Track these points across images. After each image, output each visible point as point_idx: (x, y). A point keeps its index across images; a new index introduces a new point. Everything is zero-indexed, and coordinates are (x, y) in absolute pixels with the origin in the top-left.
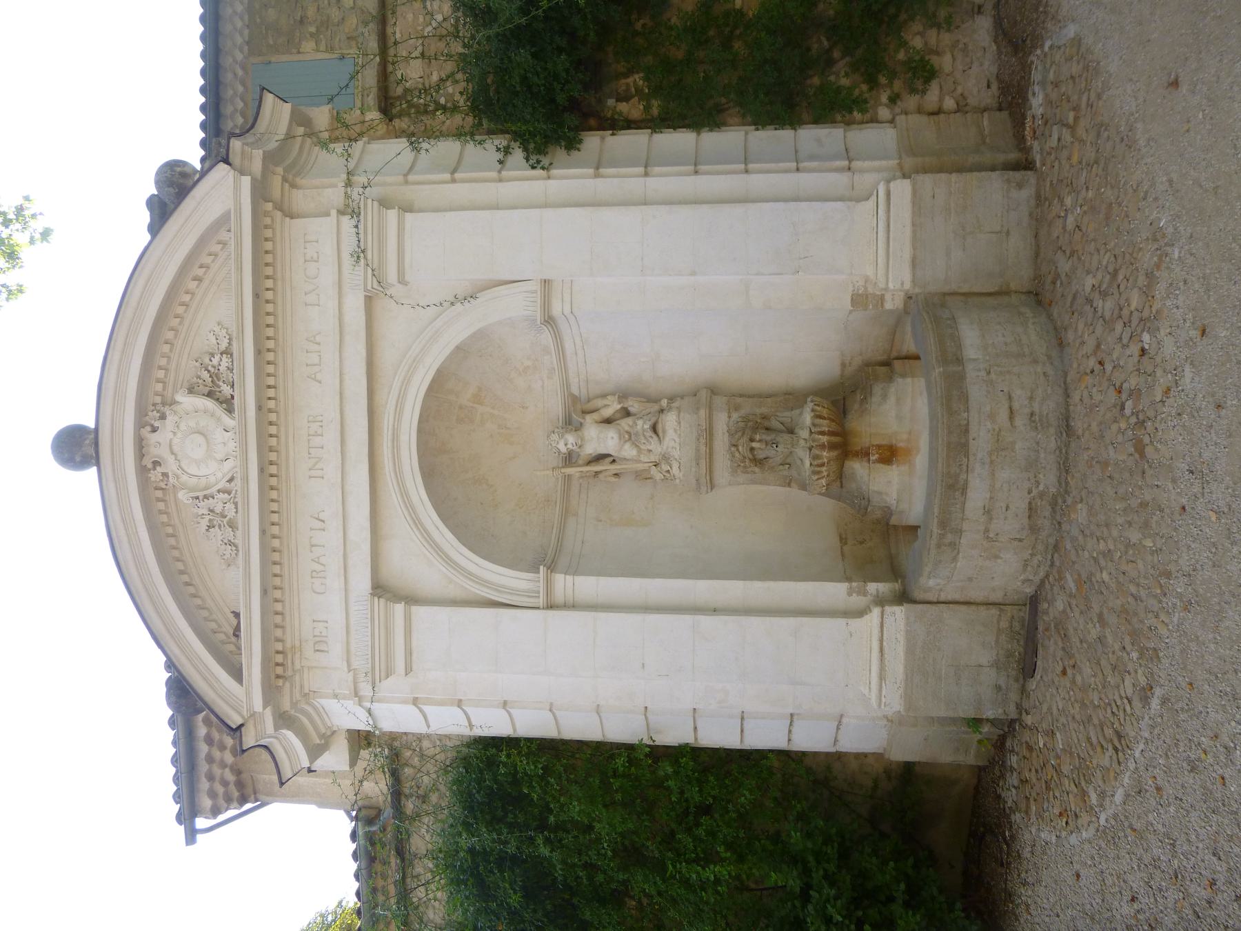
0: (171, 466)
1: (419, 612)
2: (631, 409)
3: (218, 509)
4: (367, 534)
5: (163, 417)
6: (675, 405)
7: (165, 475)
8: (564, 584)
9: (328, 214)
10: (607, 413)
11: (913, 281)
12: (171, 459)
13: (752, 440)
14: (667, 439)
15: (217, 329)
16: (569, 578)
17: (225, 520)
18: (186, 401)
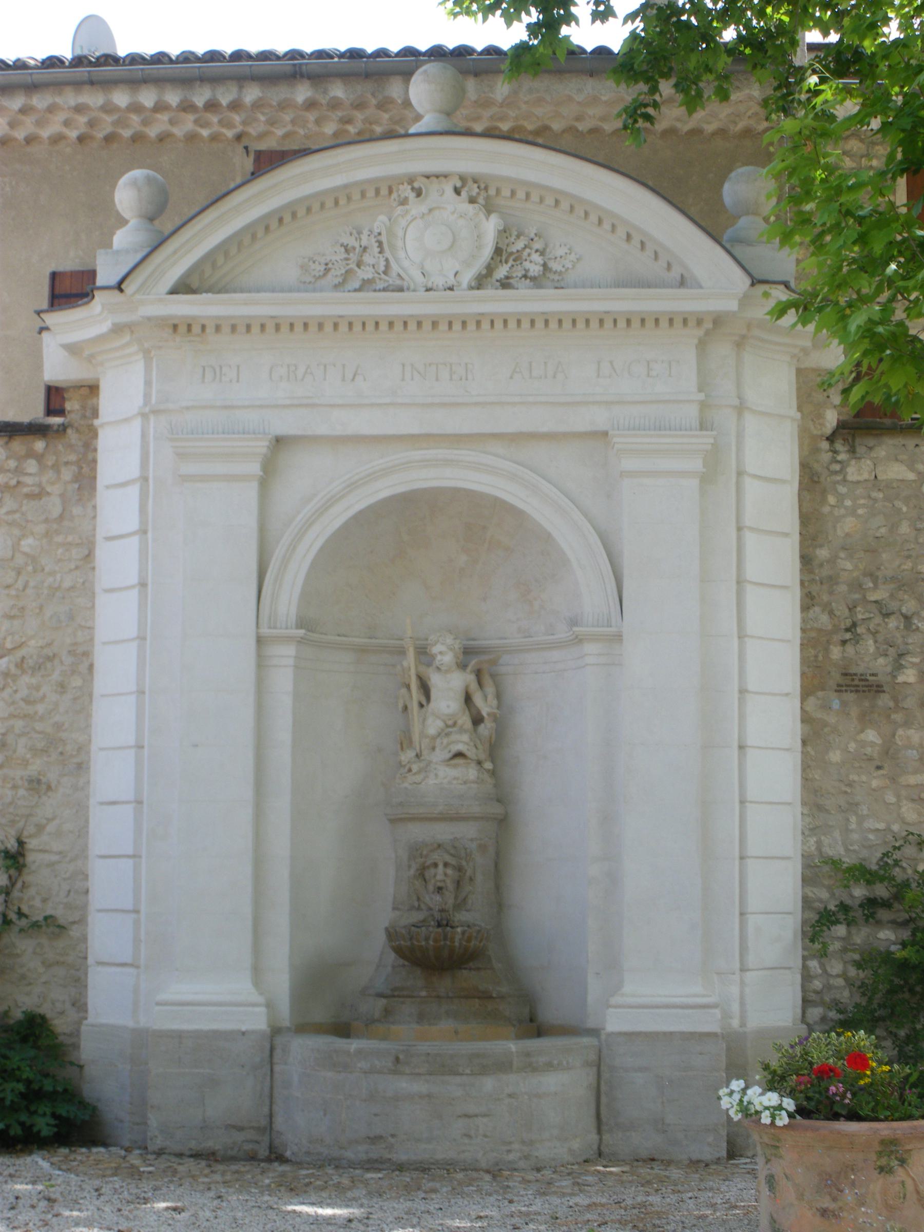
0: (416, 208)
1: (251, 491)
2: (481, 728)
3: (367, 258)
4: (339, 431)
5: (472, 201)
6: (486, 776)
7: (404, 202)
8: (284, 655)
9: (700, 390)
10: (478, 700)
11: (613, 1033)
12: (423, 209)
13: (446, 865)
14: (447, 769)
15: (573, 257)
16: (291, 661)
17: (353, 266)
18: (491, 226)
